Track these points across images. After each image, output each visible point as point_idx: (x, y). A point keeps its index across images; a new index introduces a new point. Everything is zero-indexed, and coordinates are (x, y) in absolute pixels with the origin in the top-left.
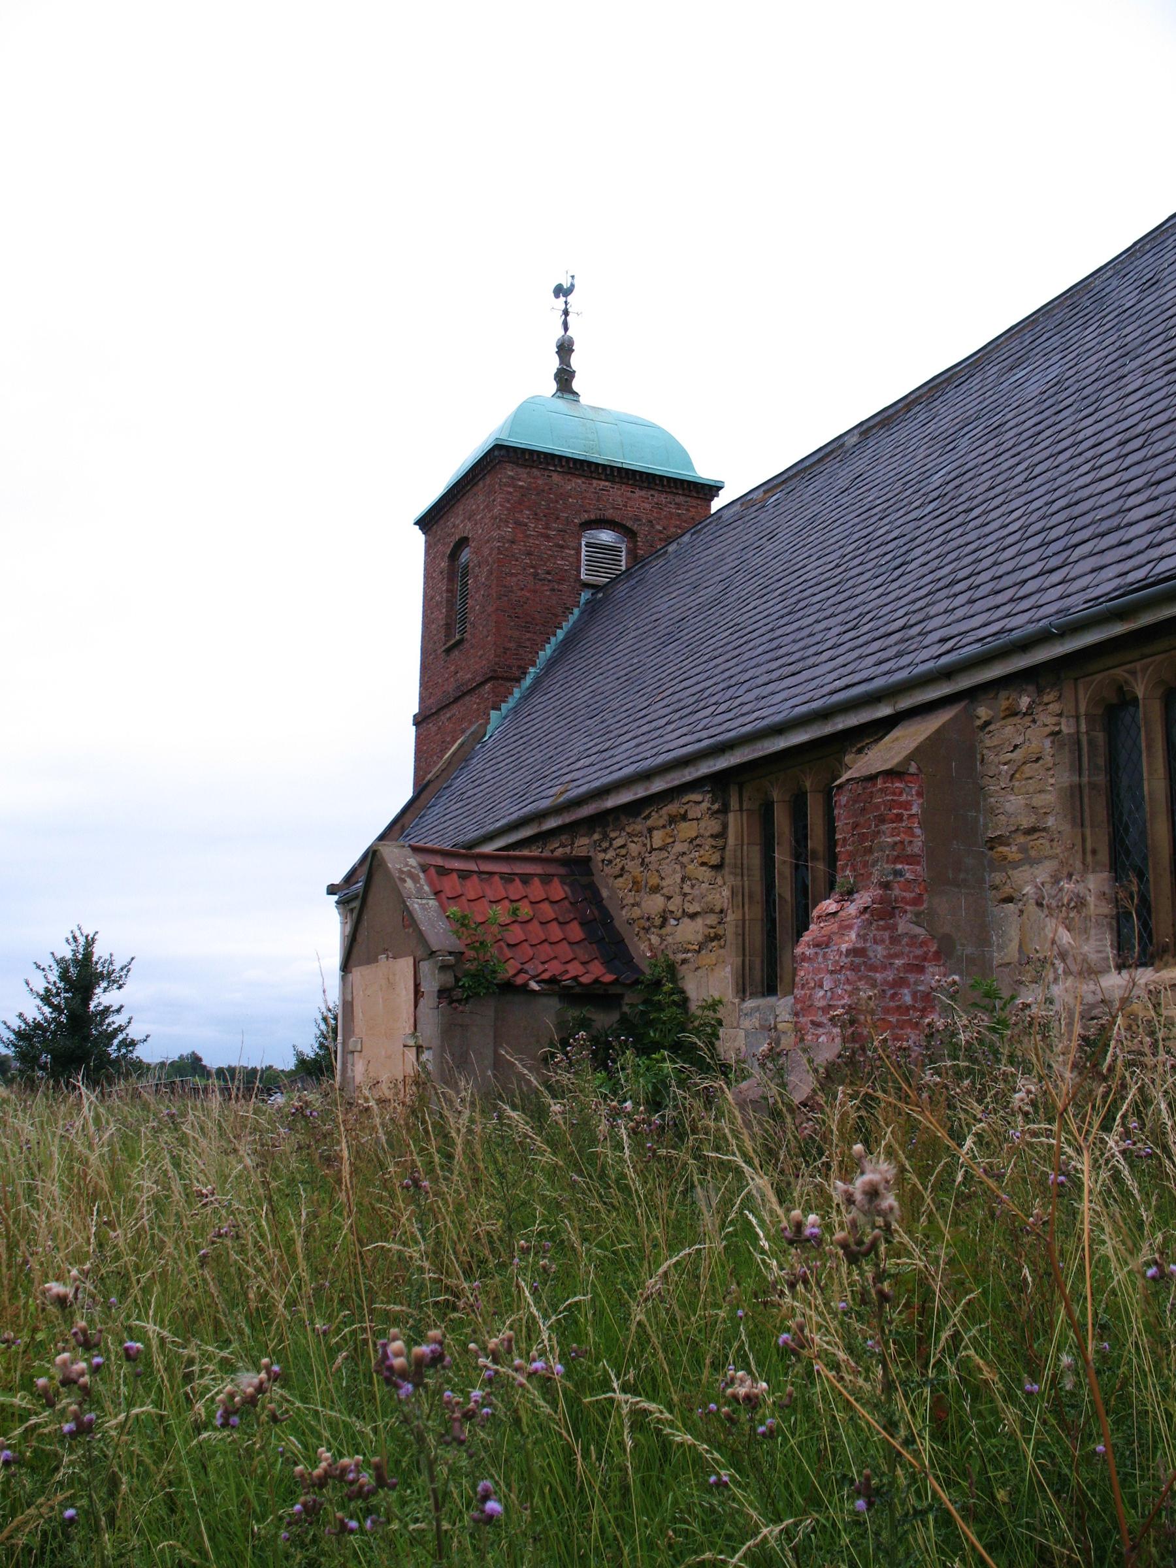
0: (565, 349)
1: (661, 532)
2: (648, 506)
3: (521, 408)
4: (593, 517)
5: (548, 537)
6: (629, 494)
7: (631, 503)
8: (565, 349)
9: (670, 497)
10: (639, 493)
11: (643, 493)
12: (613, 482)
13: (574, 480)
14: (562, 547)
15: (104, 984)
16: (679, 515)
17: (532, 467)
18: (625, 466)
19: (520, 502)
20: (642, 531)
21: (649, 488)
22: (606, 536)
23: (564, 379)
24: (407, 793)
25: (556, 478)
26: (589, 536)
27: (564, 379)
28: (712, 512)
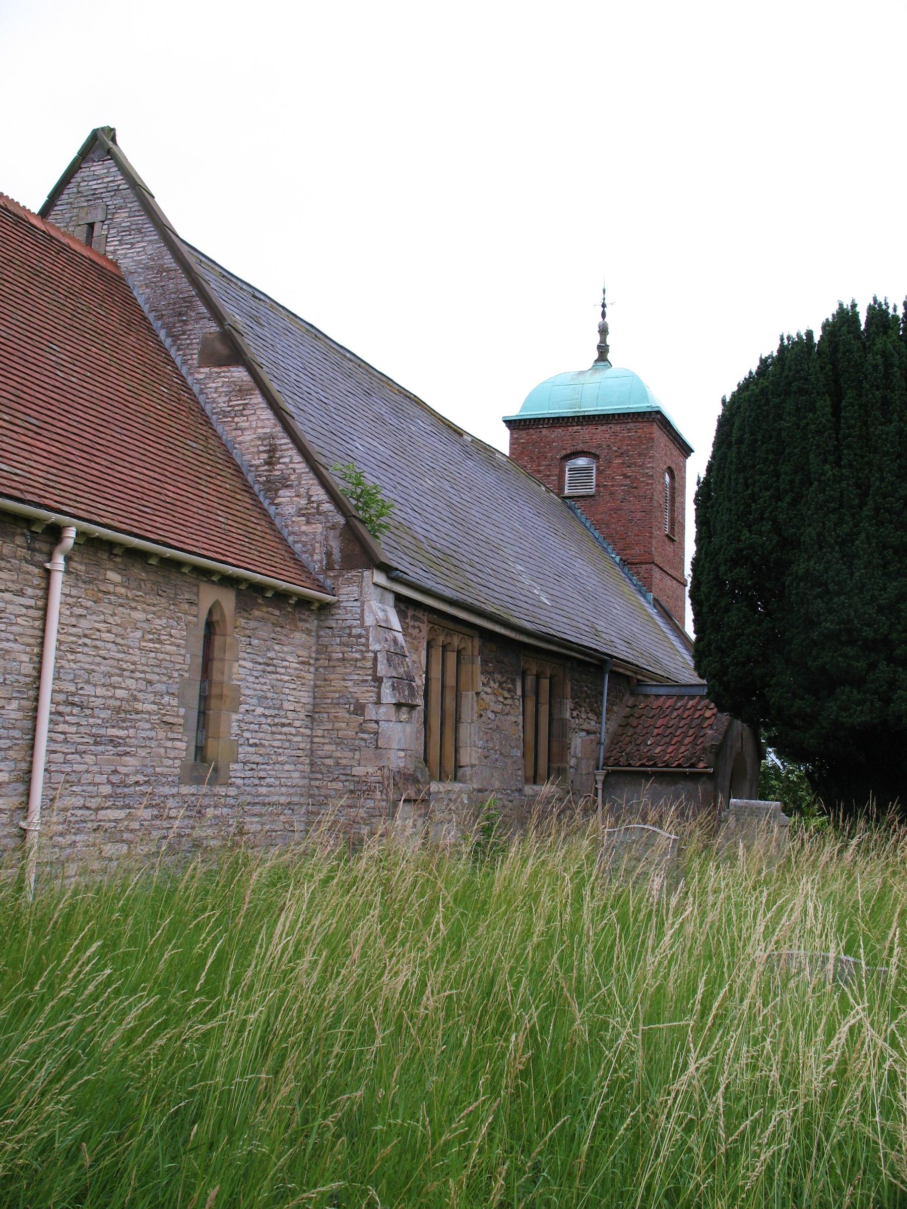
0: (603, 331)
1: (616, 451)
2: (607, 436)
3: (526, 401)
4: (569, 452)
5: (539, 472)
6: (594, 431)
7: (595, 437)
8: (603, 331)
9: (623, 426)
10: (600, 428)
11: (604, 428)
12: (582, 425)
13: (556, 430)
14: (549, 476)
15: (337, 555)
16: (629, 437)
17: (528, 429)
18: (586, 414)
19: (522, 453)
20: (603, 453)
21: (608, 424)
22: (581, 462)
23: (603, 350)
24: (187, 229)
25: (545, 432)
26: (569, 465)
27: (603, 350)
28: (506, 450)
